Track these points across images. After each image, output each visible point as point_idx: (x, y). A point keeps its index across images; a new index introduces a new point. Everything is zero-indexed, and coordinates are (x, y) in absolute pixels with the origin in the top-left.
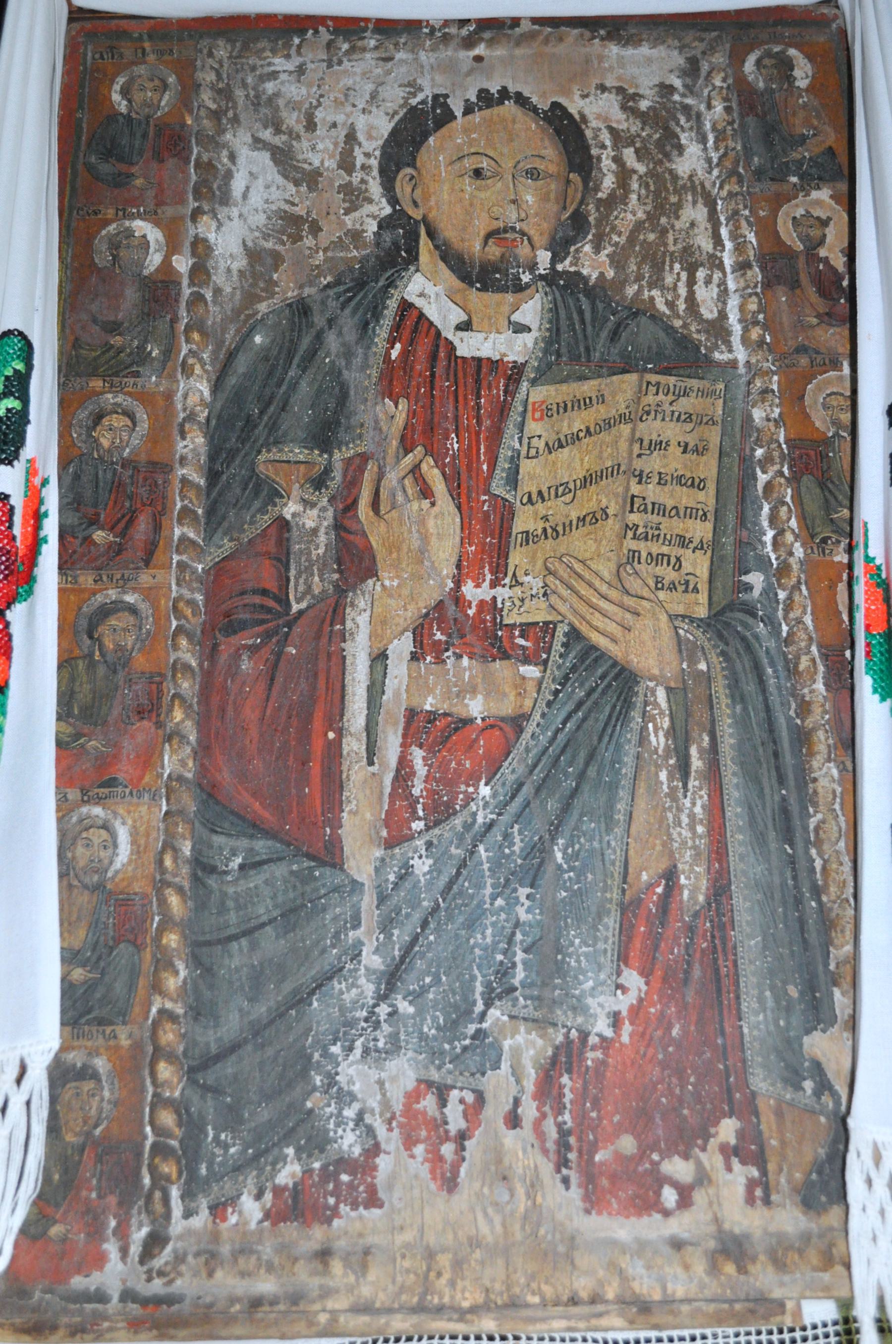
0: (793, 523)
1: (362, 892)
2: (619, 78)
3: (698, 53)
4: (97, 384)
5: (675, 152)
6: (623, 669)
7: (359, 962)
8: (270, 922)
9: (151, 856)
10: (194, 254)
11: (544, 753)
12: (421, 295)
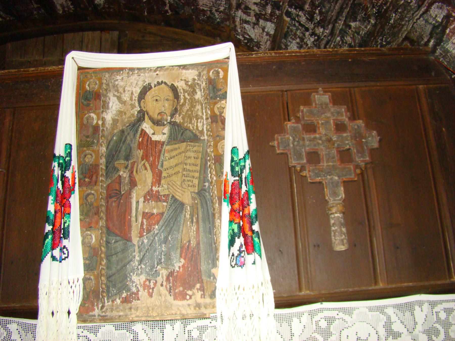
2: (185, 77)
4: (85, 149)
10: (102, 120)
12: (146, 127)
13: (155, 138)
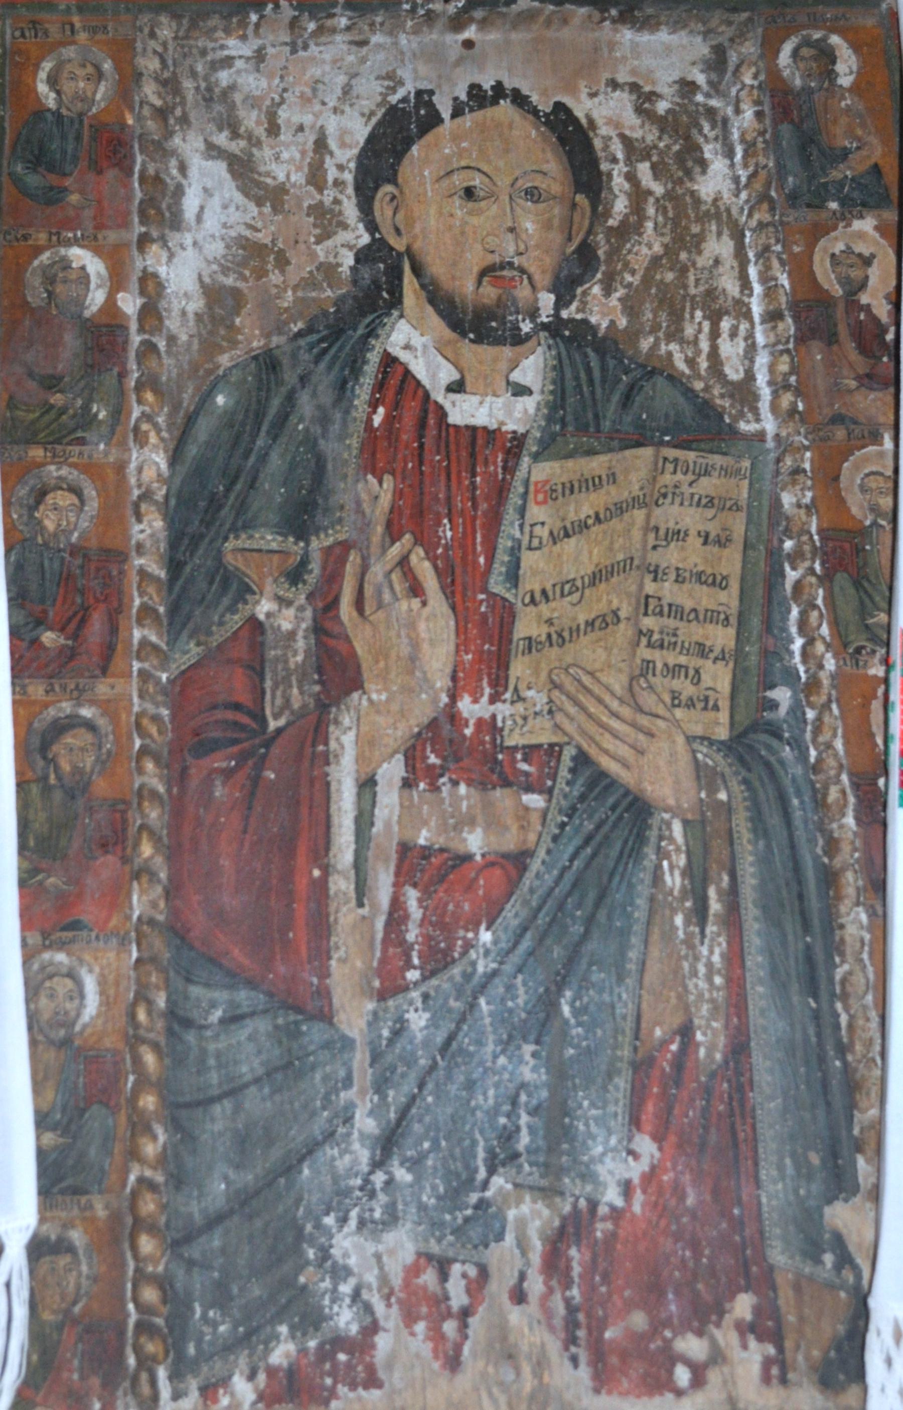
0: (825, 630)
3: (723, 39)
4: (37, 453)
5: (698, 169)
6: (636, 799)
7: (352, 1126)
8: (257, 1081)
10: (143, 292)
12: (407, 347)
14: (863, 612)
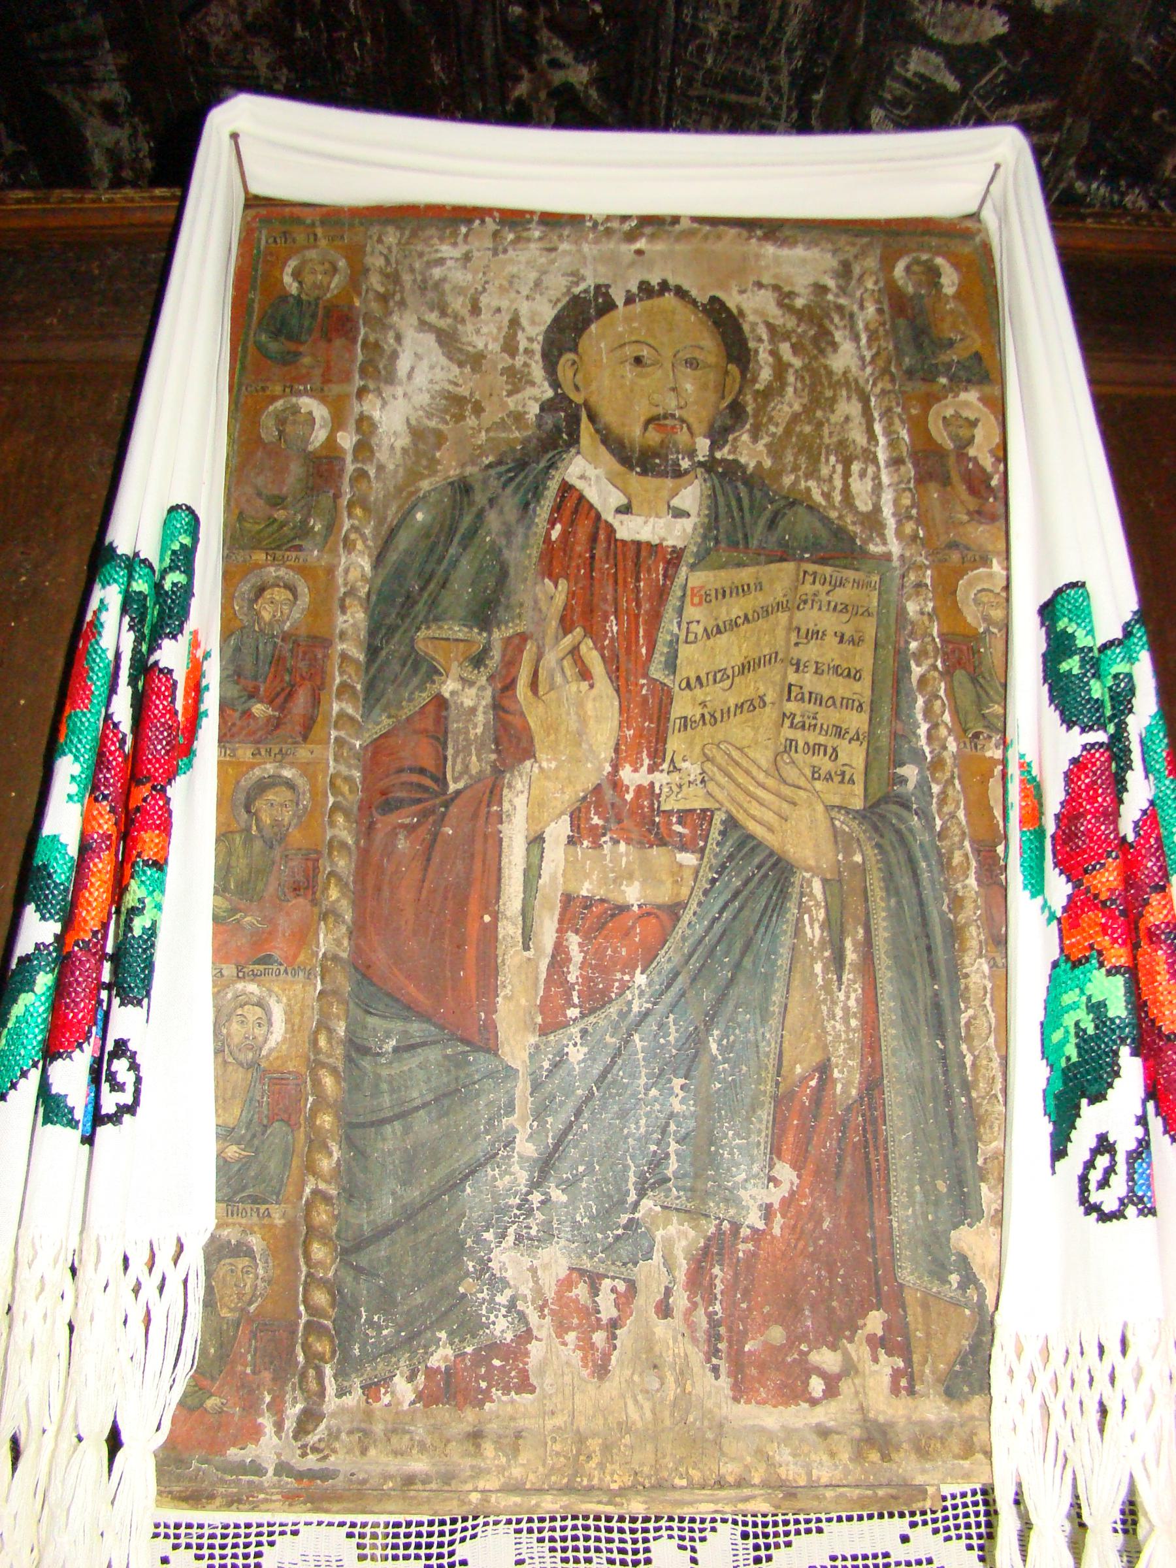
0: (947, 717)
1: (516, 1078)
2: (776, 276)
3: (849, 256)
4: (260, 556)
5: (829, 349)
6: (779, 860)
7: (513, 1149)
8: (425, 1105)
9: (304, 1037)
10: (359, 430)
11: (700, 941)
12: (582, 477)
13: (629, 529)
14: (979, 704)
